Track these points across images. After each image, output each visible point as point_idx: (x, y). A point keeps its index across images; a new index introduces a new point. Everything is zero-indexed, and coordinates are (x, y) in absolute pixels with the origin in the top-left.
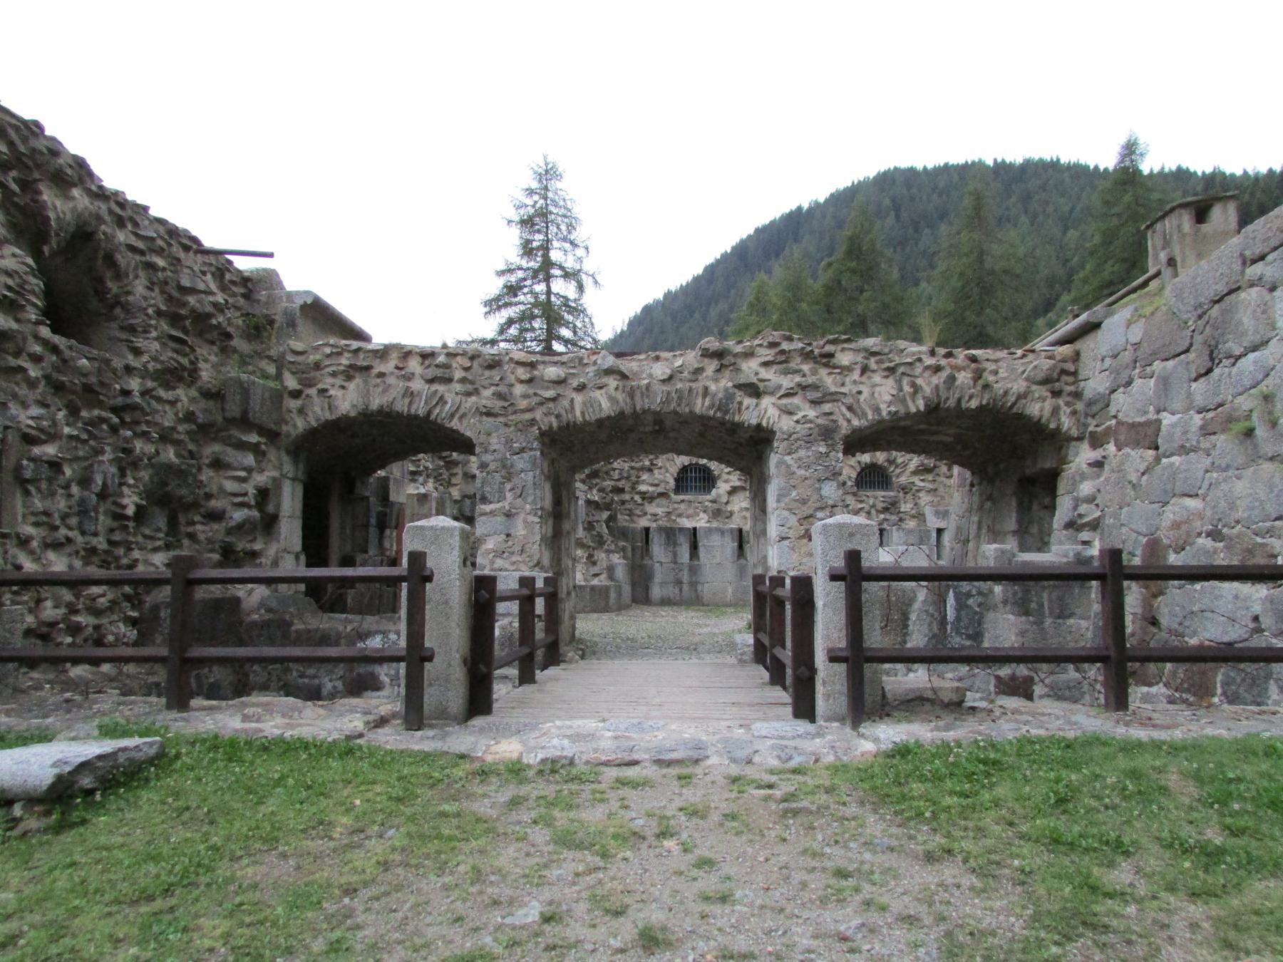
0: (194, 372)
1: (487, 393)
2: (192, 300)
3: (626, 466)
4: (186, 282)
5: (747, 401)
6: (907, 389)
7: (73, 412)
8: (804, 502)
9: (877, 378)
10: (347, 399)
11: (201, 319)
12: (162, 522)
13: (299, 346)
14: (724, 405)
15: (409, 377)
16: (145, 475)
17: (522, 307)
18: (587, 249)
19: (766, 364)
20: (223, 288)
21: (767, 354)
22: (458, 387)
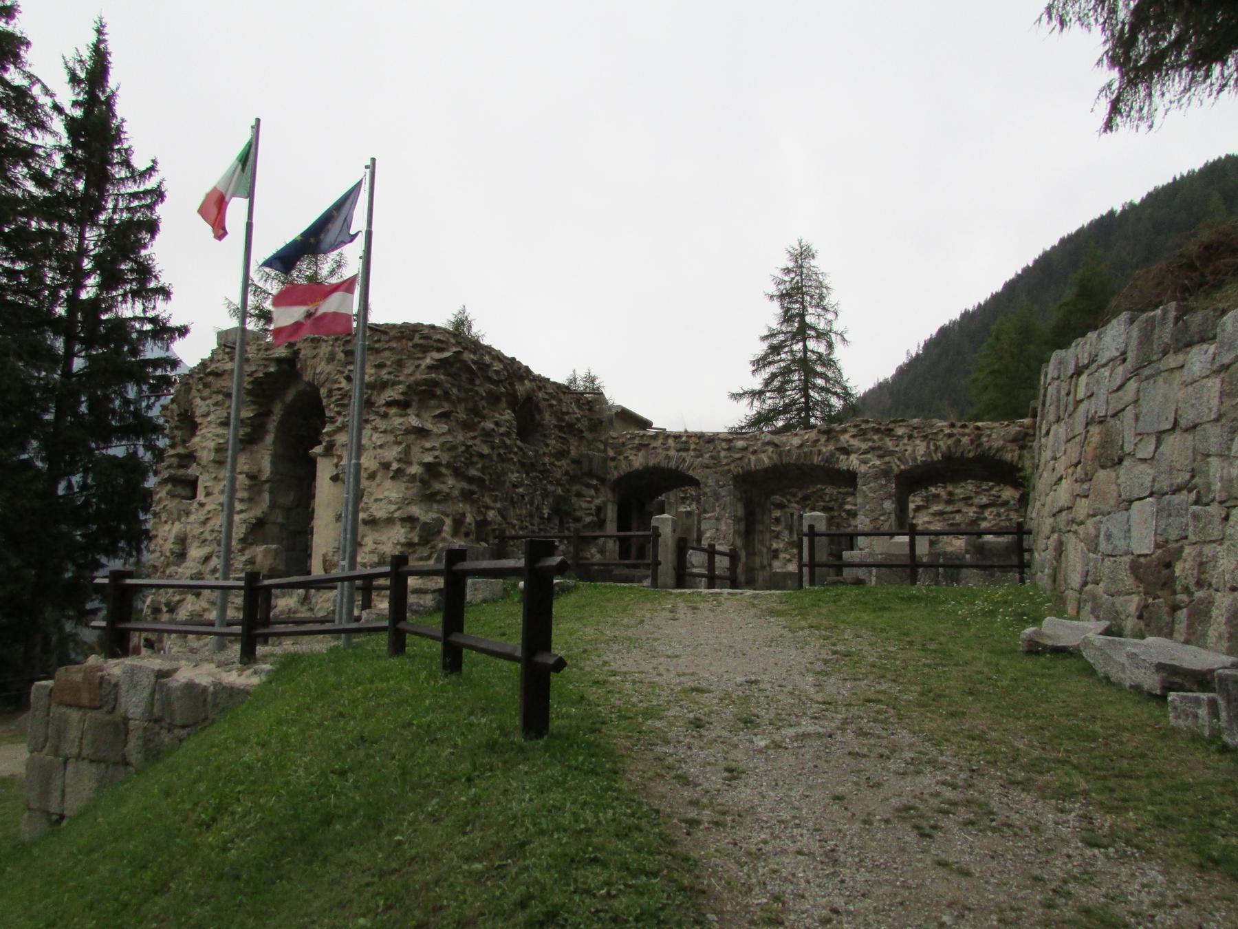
0: (568, 452)
1: (707, 456)
2: (567, 418)
3: (835, 492)
4: (564, 410)
5: (842, 457)
6: (932, 448)
7: (527, 474)
8: (873, 511)
9: (918, 442)
10: (638, 461)
11: (571, 426)
12: (557, 521)
13: (614, 434)
14: (830, 458)
15: (668, 449)
16: (551, 500)
17: (782, 364)
18: (836, 313)
19: (853, 436)
20: (579, 407)
21: (853, 431)
22: (692, 453)
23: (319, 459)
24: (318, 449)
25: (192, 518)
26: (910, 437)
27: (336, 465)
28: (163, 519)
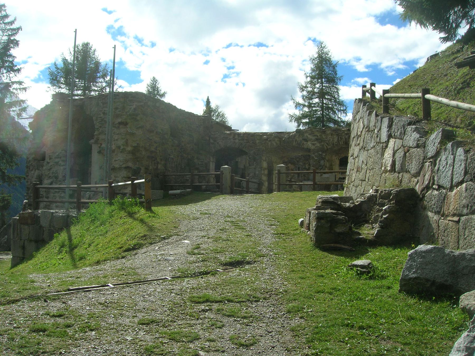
5: (305, 143)
15: (236, 139)
22: (245, 141)
23: (93, 145)
24: (92, 141)
25: (44, 168)
26: (332, 134)
27: (100, 147)
28: (31, 169)
